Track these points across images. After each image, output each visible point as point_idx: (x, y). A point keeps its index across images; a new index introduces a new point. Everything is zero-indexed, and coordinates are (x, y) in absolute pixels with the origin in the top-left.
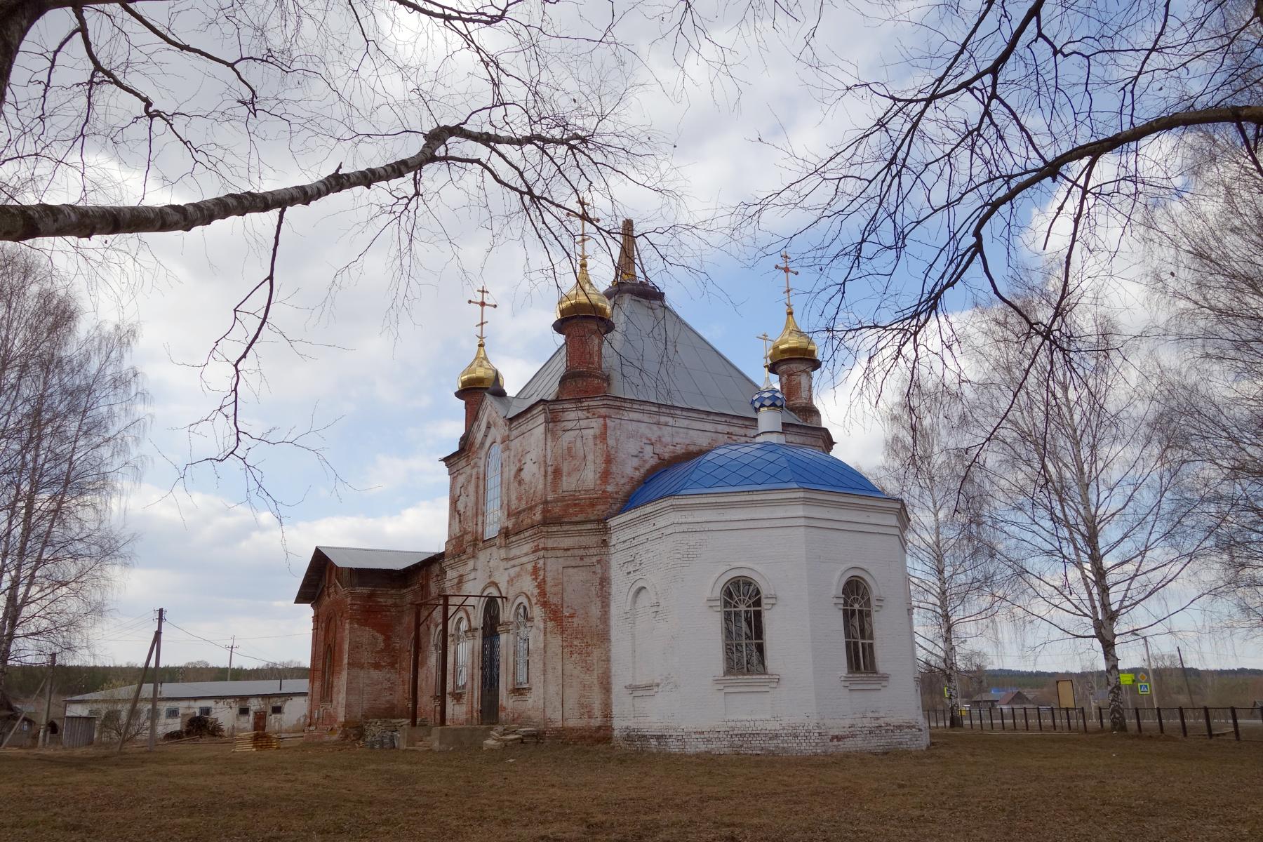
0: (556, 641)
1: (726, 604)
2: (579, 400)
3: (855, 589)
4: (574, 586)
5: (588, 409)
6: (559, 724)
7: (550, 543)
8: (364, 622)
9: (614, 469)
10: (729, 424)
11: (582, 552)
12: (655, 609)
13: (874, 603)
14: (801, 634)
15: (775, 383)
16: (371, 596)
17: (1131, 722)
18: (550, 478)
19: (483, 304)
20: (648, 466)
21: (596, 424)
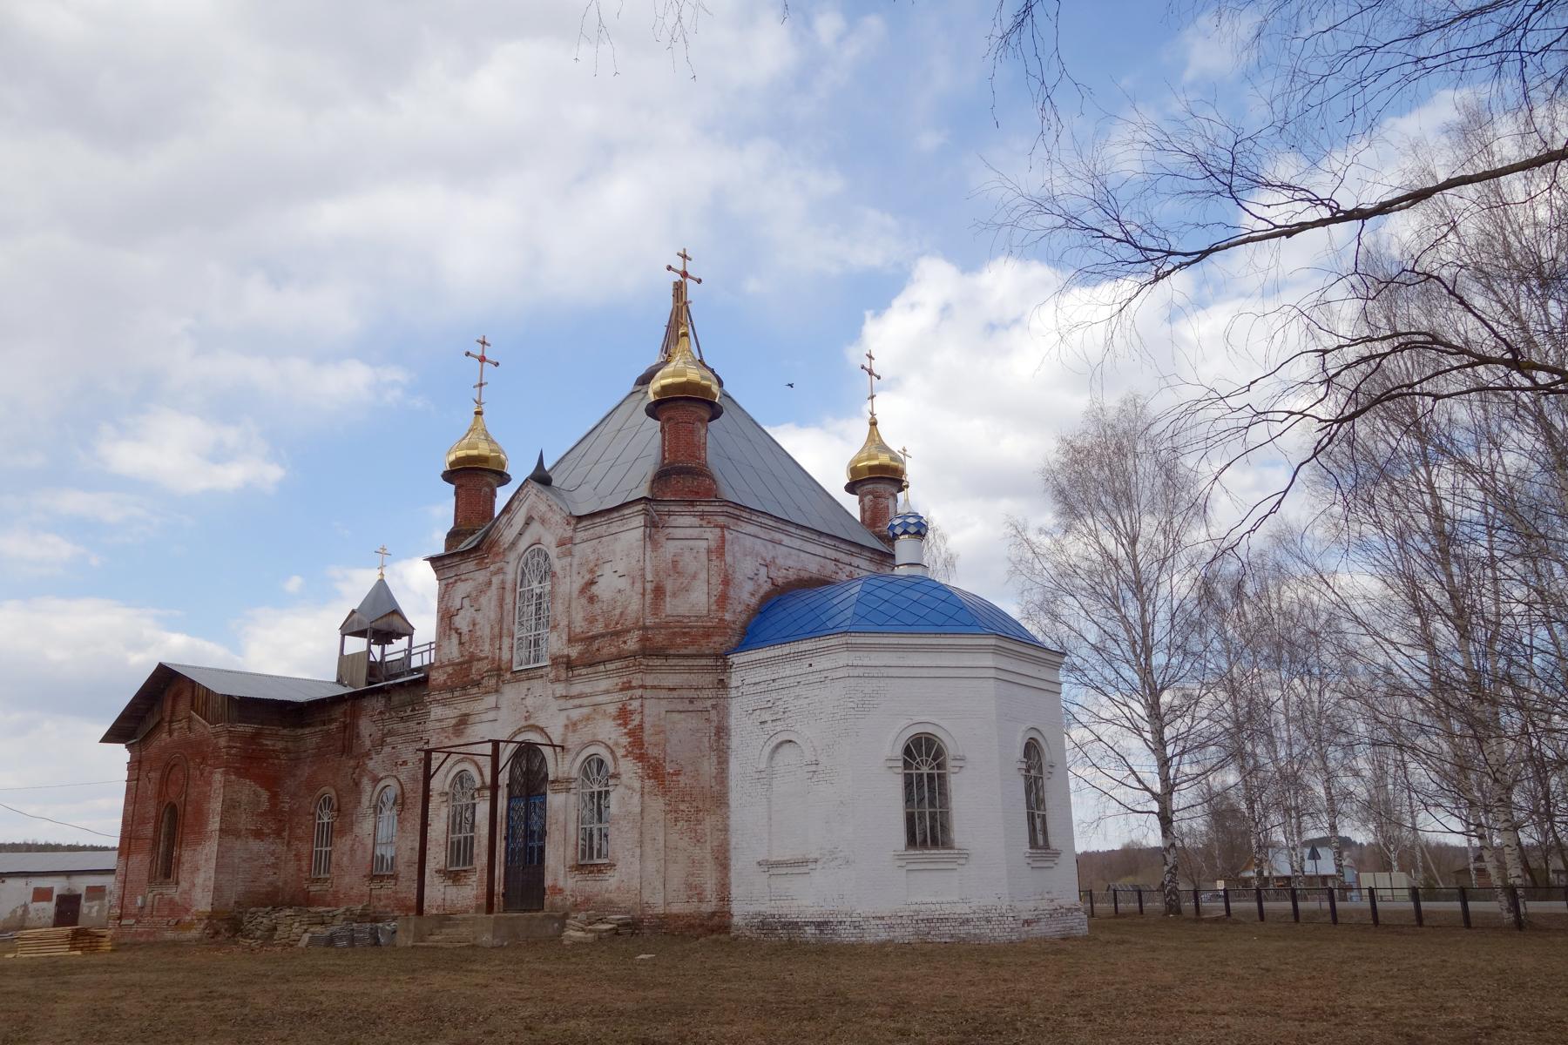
0: (657, 805)
1: (907, 765)
2: (692, 503)
3: (1032, 749)
4: (680, 736)
5: (702, 515)
6: (660, 910)
7: (650, 680)
8: (242, 773)
9: (731, 593)
10: (836, 549)
11: (692, 694)
12: (813, 768)
13: (950, 764)
14: (981, 801)
15: (852, 504)
16: (257, 735)
17: (1188, 905)
18: (649, 597)
19: (482, 359)
20: (762, 592)
21: (712, 534)
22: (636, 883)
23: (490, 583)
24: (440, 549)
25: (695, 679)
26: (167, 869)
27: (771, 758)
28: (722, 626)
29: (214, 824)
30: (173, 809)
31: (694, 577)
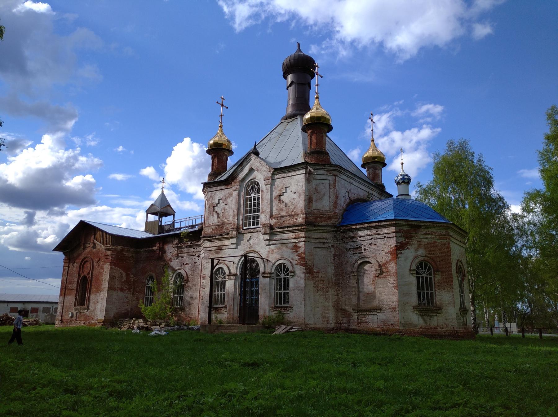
0: (311, 284)
5: (327, 170)
6: (312, 326)
9: (338, 202)
16: (123, 250)
19: (222, 105)
21: (331, 178)
22: (303, 315)
23: (232, 194)
24: (206, 180)
25: (325, 235)
26: (82, 300)
27: (358, 268)
28: (335, 215)
29: (105, 284)
30: (85, 278)
31: (324, 195)
